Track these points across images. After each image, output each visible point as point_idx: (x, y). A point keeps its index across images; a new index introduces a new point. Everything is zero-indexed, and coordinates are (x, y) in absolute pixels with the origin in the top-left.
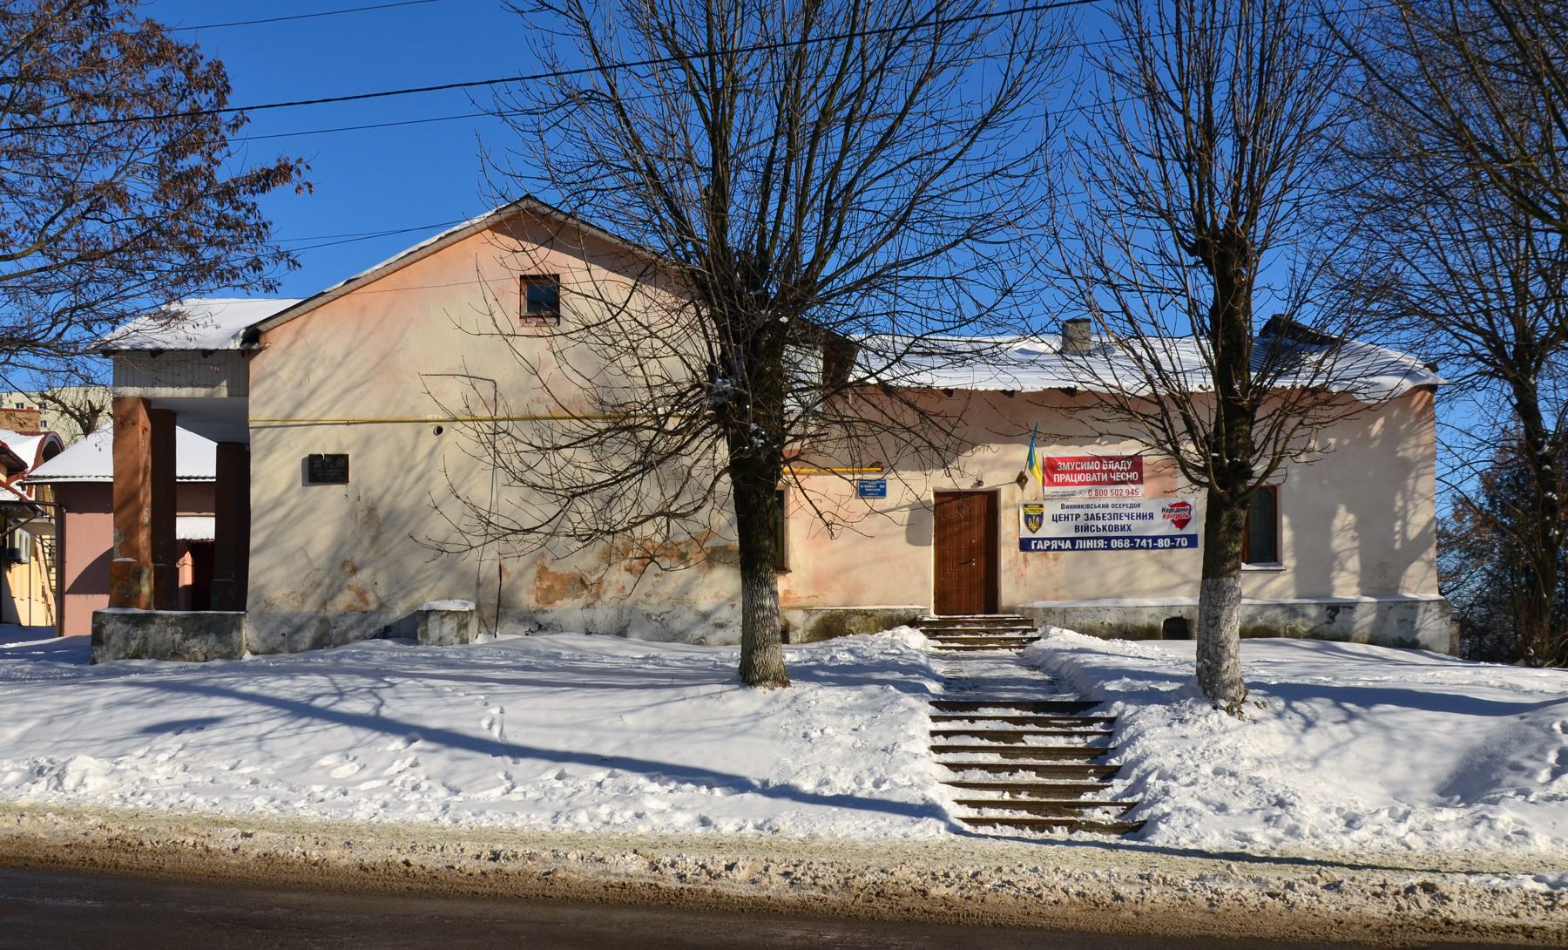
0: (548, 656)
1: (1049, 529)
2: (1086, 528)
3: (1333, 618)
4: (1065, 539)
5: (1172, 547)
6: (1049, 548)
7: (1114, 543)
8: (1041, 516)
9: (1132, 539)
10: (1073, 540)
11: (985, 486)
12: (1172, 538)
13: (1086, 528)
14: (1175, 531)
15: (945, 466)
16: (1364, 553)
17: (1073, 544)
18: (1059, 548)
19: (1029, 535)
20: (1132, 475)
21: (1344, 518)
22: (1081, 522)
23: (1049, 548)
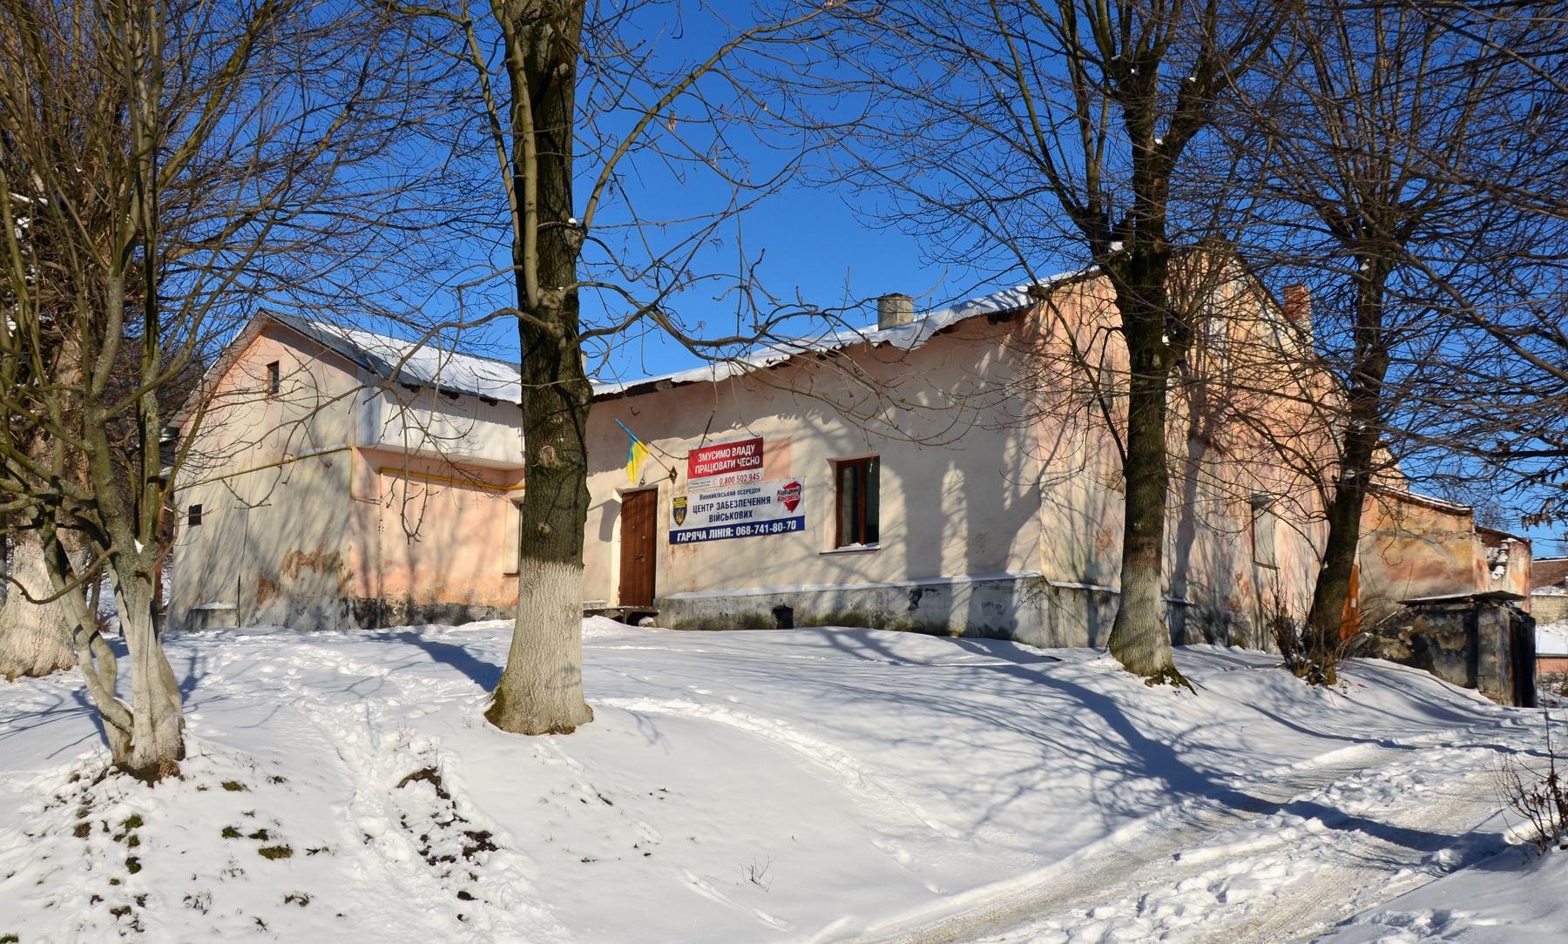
0: (174, 122)
1: (693, 521)
2: (718, 518)
3: (916, 603)
4: (701, 530)
5: (784, 531)
6: (690, 540)
7: (740, 531)
8: (685, 509)
9: (752, 525)
10: (708, 530)
11: (648, 483)
12: (784, 521)
13: (718, 518)
14: (789, 515)
15: (1168, 254)
16: (971, 517)
17: (753, 528)
18: (698, 540)
19: (677, 528)
20: (755, 461)
21: (952, 478)
22: (714, 511)
23: (690, 540)
